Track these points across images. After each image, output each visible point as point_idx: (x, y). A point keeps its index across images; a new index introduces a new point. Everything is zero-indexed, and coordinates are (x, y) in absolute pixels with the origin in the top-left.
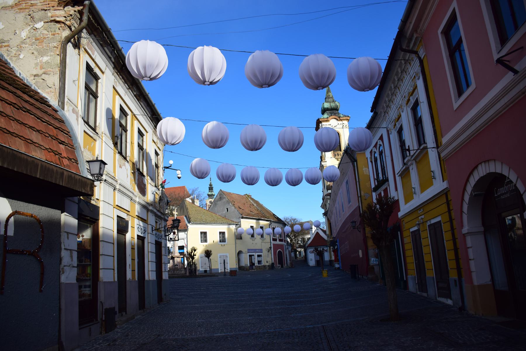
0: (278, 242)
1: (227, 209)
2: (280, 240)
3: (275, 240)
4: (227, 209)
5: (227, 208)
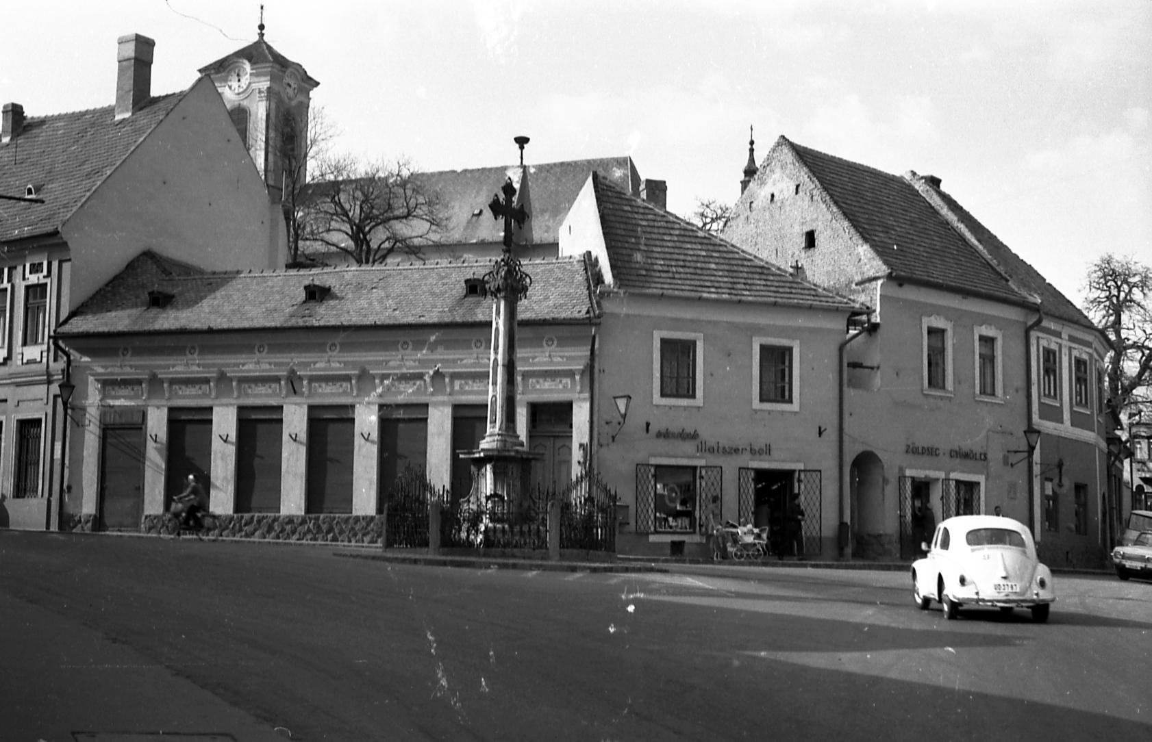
3: (1054, 414)
5: (807, 229)
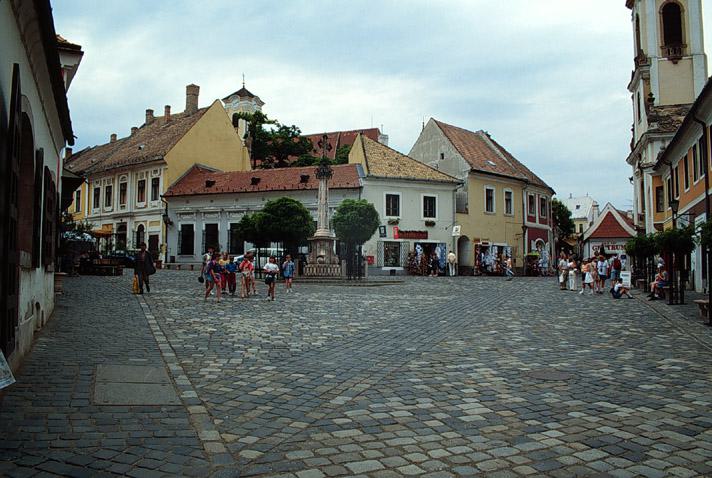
0: (537, 224)
1: (442, 155)
2: (542, 221)
4: (442, 155)
